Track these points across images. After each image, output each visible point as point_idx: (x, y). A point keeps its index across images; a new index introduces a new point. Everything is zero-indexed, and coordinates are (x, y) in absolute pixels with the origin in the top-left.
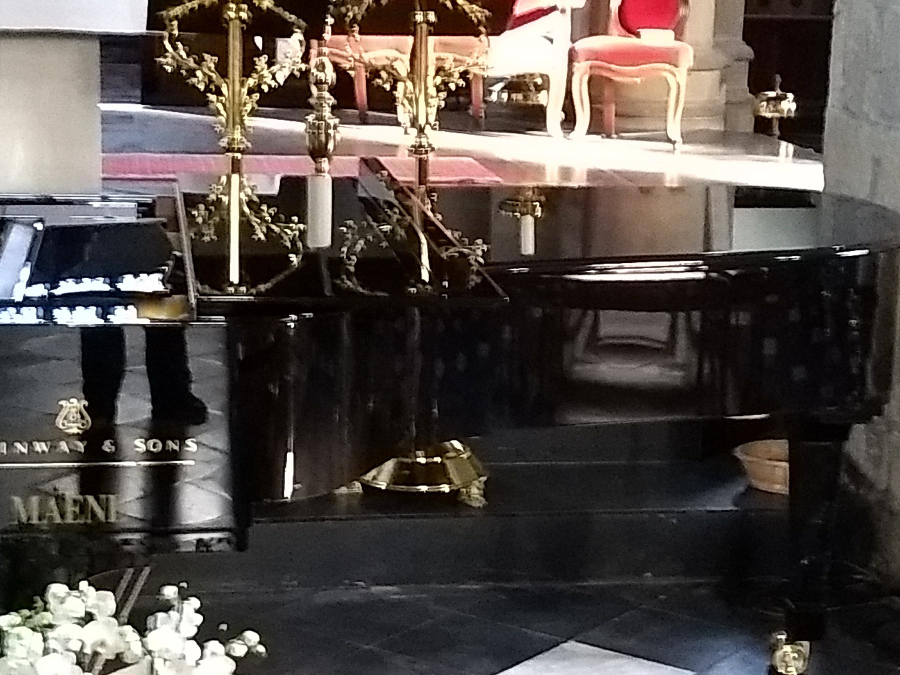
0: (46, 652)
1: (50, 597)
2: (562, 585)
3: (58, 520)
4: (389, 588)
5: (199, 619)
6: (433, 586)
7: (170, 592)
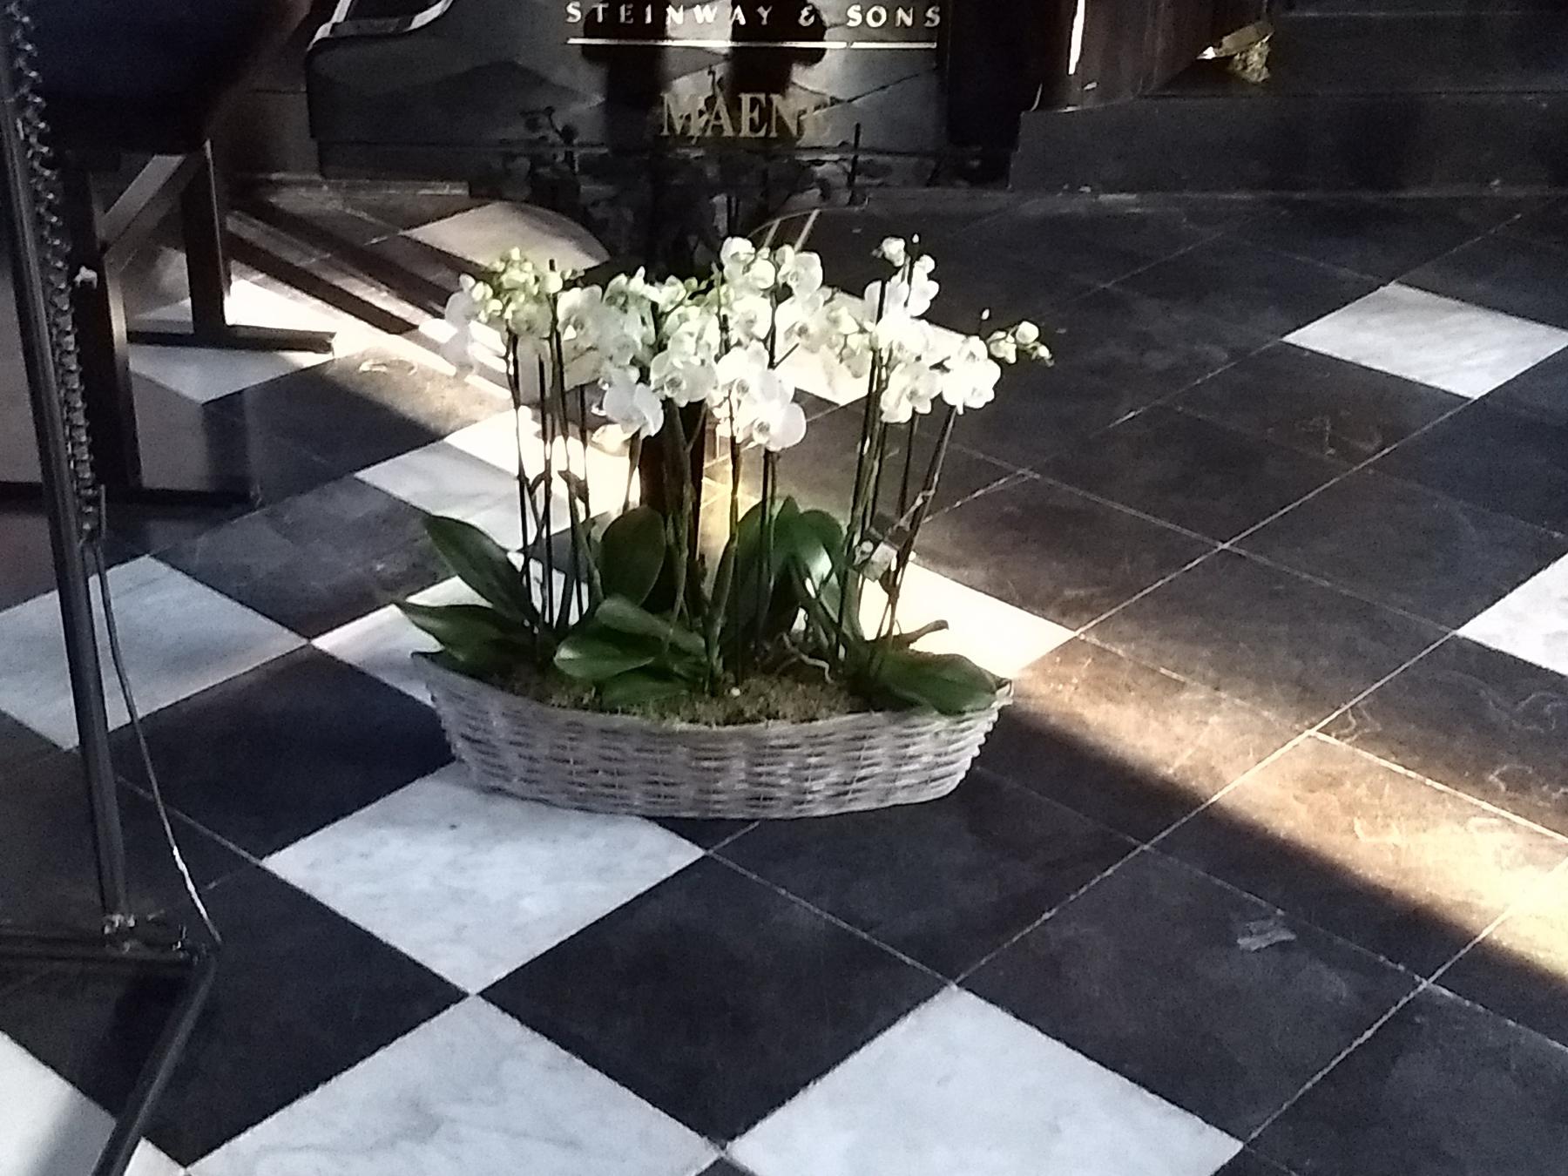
0: (726, 347)
1: (725, 256)
2: (1369, 197)
3: (728, 132)
4: (1123, 197)
5: (934, 288)
6: (1187, 194)
7: (894, 248)
